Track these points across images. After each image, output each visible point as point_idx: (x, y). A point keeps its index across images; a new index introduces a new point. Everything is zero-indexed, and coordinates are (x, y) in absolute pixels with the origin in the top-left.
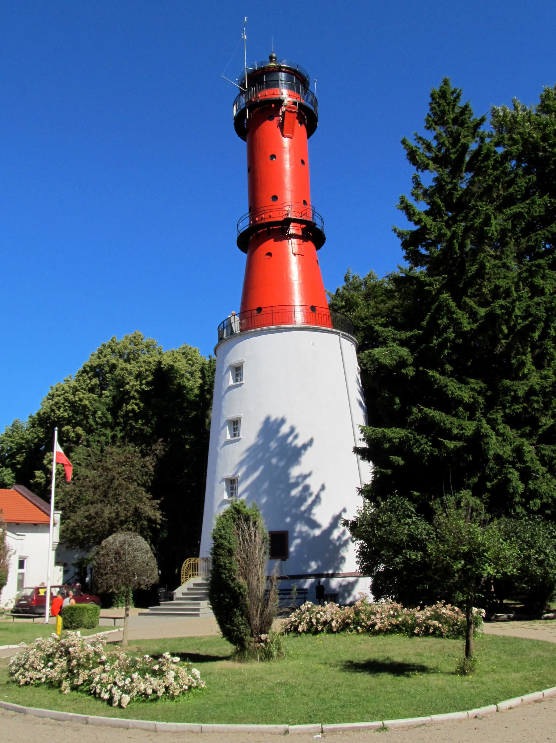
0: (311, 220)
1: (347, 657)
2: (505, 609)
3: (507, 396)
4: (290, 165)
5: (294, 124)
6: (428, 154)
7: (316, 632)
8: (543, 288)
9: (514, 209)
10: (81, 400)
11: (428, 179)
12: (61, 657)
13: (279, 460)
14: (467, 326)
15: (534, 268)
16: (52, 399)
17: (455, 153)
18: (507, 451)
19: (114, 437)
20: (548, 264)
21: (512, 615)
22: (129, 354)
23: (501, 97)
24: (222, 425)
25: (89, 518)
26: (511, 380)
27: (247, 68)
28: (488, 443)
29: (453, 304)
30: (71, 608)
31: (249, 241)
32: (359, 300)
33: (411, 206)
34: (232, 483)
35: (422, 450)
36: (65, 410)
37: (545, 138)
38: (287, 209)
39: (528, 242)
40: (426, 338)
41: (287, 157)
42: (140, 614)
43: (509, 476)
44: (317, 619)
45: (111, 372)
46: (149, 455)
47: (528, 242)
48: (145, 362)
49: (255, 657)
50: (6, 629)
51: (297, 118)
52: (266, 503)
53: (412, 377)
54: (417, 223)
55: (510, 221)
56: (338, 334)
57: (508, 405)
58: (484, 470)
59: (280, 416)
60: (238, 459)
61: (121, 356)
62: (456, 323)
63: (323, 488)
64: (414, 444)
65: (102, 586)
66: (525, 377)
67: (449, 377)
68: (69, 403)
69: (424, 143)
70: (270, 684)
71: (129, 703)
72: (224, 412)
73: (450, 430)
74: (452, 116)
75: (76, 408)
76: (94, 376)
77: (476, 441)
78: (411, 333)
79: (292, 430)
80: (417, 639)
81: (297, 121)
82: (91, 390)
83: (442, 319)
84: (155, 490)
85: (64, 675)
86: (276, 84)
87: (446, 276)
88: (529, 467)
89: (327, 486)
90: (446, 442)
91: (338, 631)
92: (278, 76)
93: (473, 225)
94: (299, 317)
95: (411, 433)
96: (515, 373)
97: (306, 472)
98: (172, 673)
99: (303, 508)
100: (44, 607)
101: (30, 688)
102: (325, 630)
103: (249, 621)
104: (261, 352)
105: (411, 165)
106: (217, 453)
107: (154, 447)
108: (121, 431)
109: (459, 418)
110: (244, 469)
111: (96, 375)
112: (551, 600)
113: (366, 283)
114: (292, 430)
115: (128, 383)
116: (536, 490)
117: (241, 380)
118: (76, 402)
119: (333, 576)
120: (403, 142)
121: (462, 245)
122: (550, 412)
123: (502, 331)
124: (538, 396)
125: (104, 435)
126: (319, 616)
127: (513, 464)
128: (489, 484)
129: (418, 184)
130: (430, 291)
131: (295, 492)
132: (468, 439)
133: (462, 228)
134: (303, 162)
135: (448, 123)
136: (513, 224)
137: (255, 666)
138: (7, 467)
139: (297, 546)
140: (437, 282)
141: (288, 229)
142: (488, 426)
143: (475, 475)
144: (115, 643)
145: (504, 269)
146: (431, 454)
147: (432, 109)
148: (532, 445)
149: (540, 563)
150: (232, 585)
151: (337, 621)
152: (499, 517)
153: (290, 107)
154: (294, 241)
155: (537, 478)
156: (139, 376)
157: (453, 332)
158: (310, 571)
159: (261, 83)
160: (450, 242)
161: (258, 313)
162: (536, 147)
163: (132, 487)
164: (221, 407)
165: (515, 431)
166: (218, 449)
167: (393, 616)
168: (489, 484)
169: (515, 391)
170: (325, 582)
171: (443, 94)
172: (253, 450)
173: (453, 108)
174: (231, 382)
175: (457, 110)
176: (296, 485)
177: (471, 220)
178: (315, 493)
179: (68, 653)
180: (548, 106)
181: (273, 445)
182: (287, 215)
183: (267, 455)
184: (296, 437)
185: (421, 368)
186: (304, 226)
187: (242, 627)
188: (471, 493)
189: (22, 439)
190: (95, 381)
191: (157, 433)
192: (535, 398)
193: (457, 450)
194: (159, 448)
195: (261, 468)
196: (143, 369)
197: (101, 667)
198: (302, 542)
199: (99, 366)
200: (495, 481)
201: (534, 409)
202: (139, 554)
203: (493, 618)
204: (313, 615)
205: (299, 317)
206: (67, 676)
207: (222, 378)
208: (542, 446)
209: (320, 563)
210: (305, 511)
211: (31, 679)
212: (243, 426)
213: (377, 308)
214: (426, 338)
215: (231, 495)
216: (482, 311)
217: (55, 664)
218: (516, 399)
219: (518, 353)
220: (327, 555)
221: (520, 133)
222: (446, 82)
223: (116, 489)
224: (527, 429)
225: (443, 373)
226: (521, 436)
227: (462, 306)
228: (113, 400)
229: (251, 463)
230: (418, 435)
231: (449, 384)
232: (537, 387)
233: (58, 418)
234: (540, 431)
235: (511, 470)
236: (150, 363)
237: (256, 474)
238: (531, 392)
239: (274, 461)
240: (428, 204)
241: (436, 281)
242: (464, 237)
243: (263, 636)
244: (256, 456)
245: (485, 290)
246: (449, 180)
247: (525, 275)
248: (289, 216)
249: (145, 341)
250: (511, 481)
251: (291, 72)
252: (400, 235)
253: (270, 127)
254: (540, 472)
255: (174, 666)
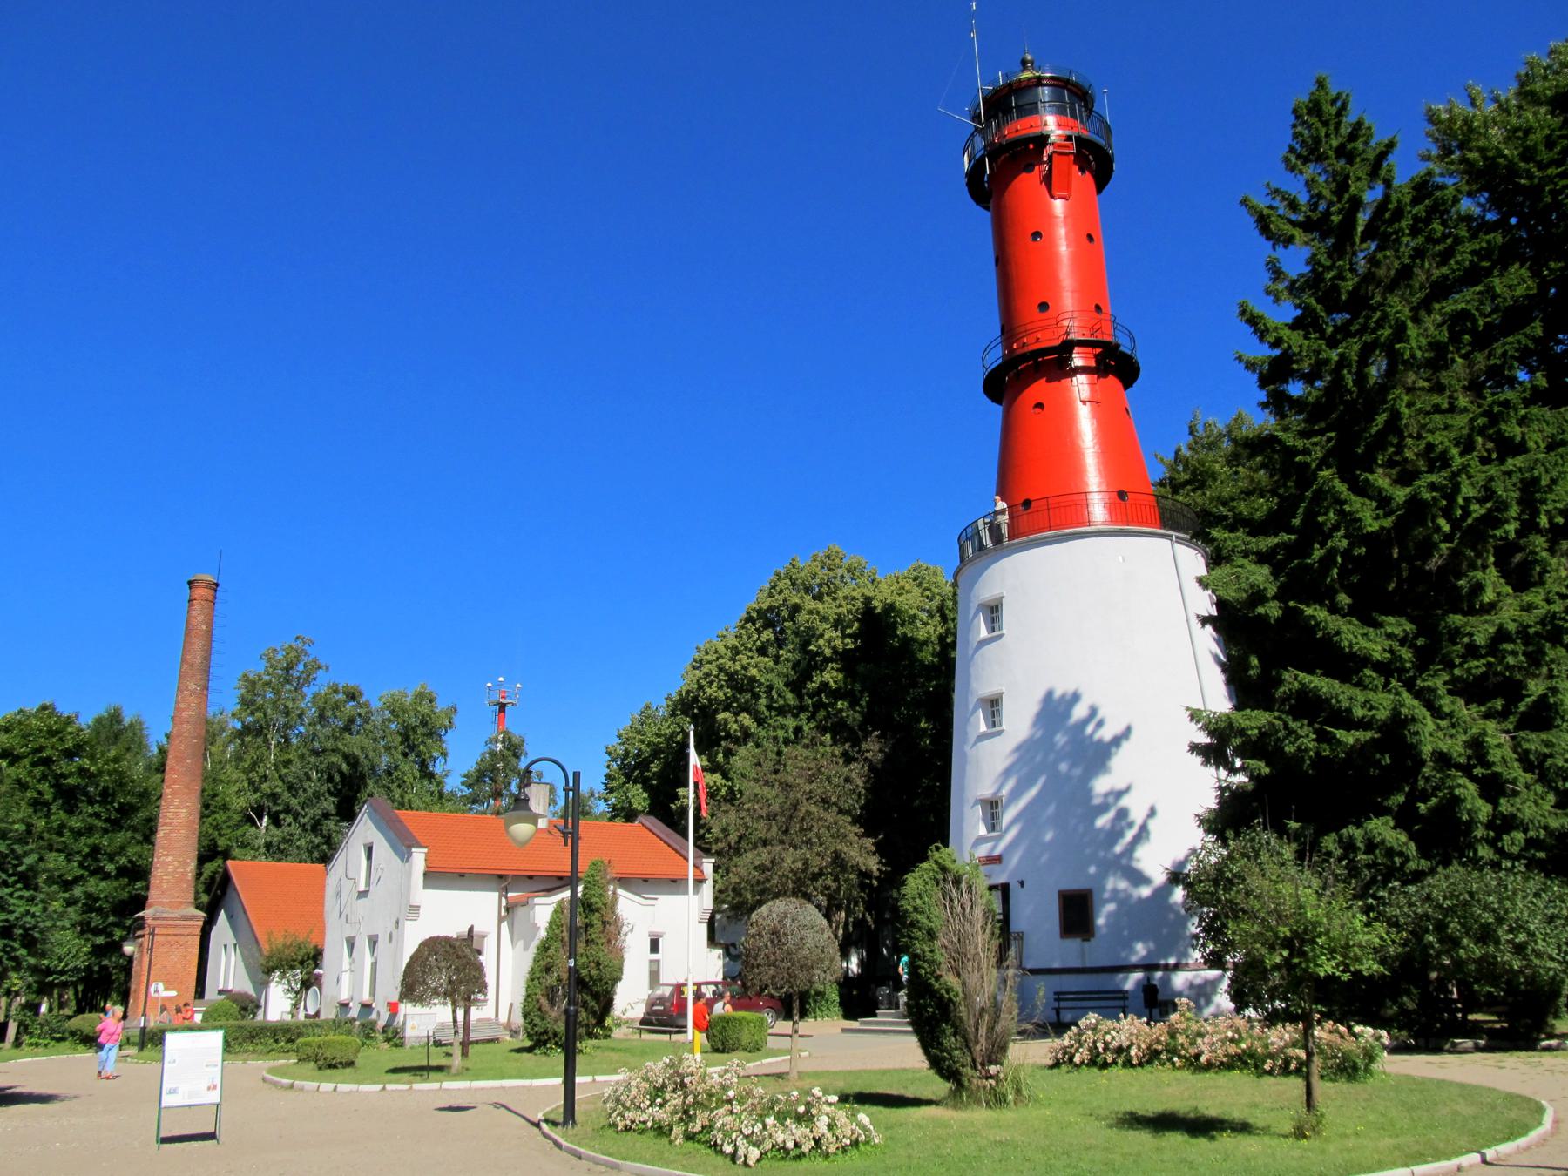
0: (1112, 340)
1: (1128, 1107)
2: (1472, 1031)
3: (1455, 644)
4: (1068, 246)
5: (1069, 174)
6: (1293, 217)
7: (1105, 1065)
8: (1523, 440)
9: (1453, 304)
10: (745, 669)
11: (1296, 260)
12: (674, 1091)
13: (1072, 766)
14: (1371, 524)
15: (1496, 409)
16: (699, 668)
17: (1340, 211)
18: (1456, 747)
19: (798, 730)
20: (1524, 400)
21: (1482, 1042)
22: (820, 585)
23: (1428, 96)
24: (971, 707)
25: (761, 868)
26: (1465, 614)
27: (982, 87)
28: (1417, 733)
29: (1341, 488)
30: (721, 1018)
31: (1003, 384)
32: (1217, 466)
33: (1262, 317)
34: (992, 807)
35: (1299, 748)
36: (721, 688)
37: (1528, 154)
38: (1066, 323)
39: (1488, 358)
40: (1300, 549)
41: (1062, 232)
42: (844, 1030)
43: (1457, 792)
44: (1106, 1044)
45: (792, 618)
46: (856, 760)
47: (1488, 358)
48: (846, 598)
49: (978, 1102)
50: (625, 1050)
51: (1075, 162)
52: (1052, 841)
53: (1278, 620)
54: (1277, 343)
55: (1445, 328)
56: (1169, 537)
57: (1457, 661)
58: (1416, 781)
59: (1070, 689)
60: (1001, 764)
61: (808, 590)
62: (1350, 521)
63: (1152, 812)
64: (1285, 738)
65: (753, 985)
66: (1491, 607)
67: (1344, 616)
68: (727, 674)
69: (1284, 199)
70: (983, 1143)
71: (758, 1160)
72: (974, 685)
73: (1349, 711)
74: (1335, 143)
75: (740, 684)
76: (766, 627)
77: (1395, 731)
78: (1276, 540)
79: (1093, 711)
80: (1268, 1080)
81: (1076, 168)
82: (762, 651)
83: (1325, 514)
84: (869, 821)
85: (676, 1118)
86: (1032, 109)
87: (1333, 434)
88: (1497, 775)
89: (1159, 809)
90: (1340, 734)
91: (1140, 1064)
92: (1037, 95)
93: (1377, 339)
94: (1098, 511)
95: (1279, 718)
96: (1471, 603)
97: (1121, 785)
98: (825, 1120)
99: (1118, 849)
100: (685, 1016)
101: (631, 1134)
102: (1120, 1062)
103: (968, 1046)
104: (1032, 579)
105: (1263, 238)
106: (964, 755)
107: (864, 746)
108: (809, 719)
109: (1365, 688)
110: (1011, 783)
111: (769, 624)
112: (1557, 1016)
113: (1230, 432)
114: (1093, 711)
115: (822, 636)
116: (1514, 816)
117: (1000, 628)
118: (736, 672)
119: (1177, 967)
120: (1244, 202)
121: (1361, 378)
122: (1545, 670)
123: (1438, 529)
124: (1513, 642)
125: (782, 727)
126: (1108, 1038)
127: (1467, 770)
128: (1422, 806)
129: (1277, 274)
130: (1307, 465)
131: (1102, 821)
132: (1384, 727)
133: (1356, 347)
134: (1090, 238)
135: (1327, 158)
136: (1450, 331)
137: (979, 1115)
138: (635, 782)
139: (1110, 915)
140: (1317, 448)
141: (1070, 358)
142: (1416, 703)
143: (1400, 790)
144: (780, 1076)
145: (1432, 415)
146: (1318, 754)
147: (1296, 136)
148: (1507, 732)
149: (1519, 949)
150: (937, 986)
151: (1139, 1048)
152: (1446, 864)
153: (1060, 146)
154: (1082, 379)
155: (1515, 793)
156: (838, 623)
157: (1345, 537)
158: (1134, 959)
159: (1007, 111)
160: (1337, 371)
161: (1034, 507)
162: (1512, 170)
163: (830, 816)
164: (968, 676)
165: (1474, 708)
166: (967, 748)
167: (1232, 1040)
168: (1422, 806)
169: (1471, 635)
170: (1162, 978)
171: (1315, 108)
172: (1025, 750)
173: (1337, 128)
174: (984, 633)
175: (1345, 130)
176: (1103, 808)
177: (1374, 331)
178: (1139, 822)
179: (683, 1085)
180: (1532, 93)
181: (1060, 739)
182: (1068, 333)
183: (1052, 757)
184: (1100, 724)
185: (1292, 604)
186: (1098, 351)
187: (957, 1053)
188: (1392, 824)
189: (658, 736)
190: (768, 635)
191: (872, 720)
192: (1509, 647)
193: (1361, 750)
194: (873, 747)
195: (1042, 780)
196: (844, 610)
197: (727, 1107)
198: (1119, 909)
199: (771, 609)
200: (1434, 800)
201: (1508, 667)
202: (809, 934)
203: (1447, 1047)
204: (1099, 1036)
205: (1098, 511)
206: (681, 1119)
207: (969, 626)
208: (1522, 734)
209: (1152, 945)
210: (1122, 854)
211: (633, 1122)
212: (1007, 707)
213: (1252, 480)
214: (1300, 549)
215: (992, 828)
216: (1401, 494)
217: (665, 1102)
218: (1472, 651)
219: (1473, 567)
220: (1165, 931)
221: (1481, 150)
222: (1321, 84)
223: (803, 819)
224: (1498, 704)
225: (1334, 610)
226: (1487, 716)
227: (1361, 489)
228: (793, 668)
229: (1025, 770)
230: (1295, 720)
231: (1344, 628)
232: (1512, 627)
233: (709, 699)
234: (1522, 707)
235: (1460, 781)
236: (854, 598)
237: (1033, 792)
238: (1502, 635)
239: (1063, 767)
240: (1297, 306)
241: (1316, 444)
242: (1364, 361)
243: (993, 1069)
244: (1030, 759)
245: (1409, 454)
246: (1328, 263)
247: (1481, 421)
248: (1071, 337)
249: (845, 563)
250: (1464, 801)
251: (1060, 84)
252: (1251, 366)
253: (1028, 183)
254: (1522, 781)
255: (826, 1109)
